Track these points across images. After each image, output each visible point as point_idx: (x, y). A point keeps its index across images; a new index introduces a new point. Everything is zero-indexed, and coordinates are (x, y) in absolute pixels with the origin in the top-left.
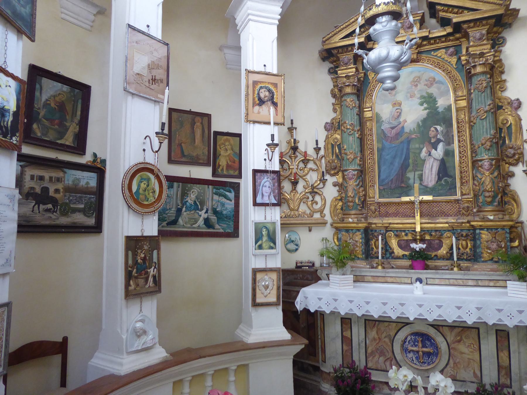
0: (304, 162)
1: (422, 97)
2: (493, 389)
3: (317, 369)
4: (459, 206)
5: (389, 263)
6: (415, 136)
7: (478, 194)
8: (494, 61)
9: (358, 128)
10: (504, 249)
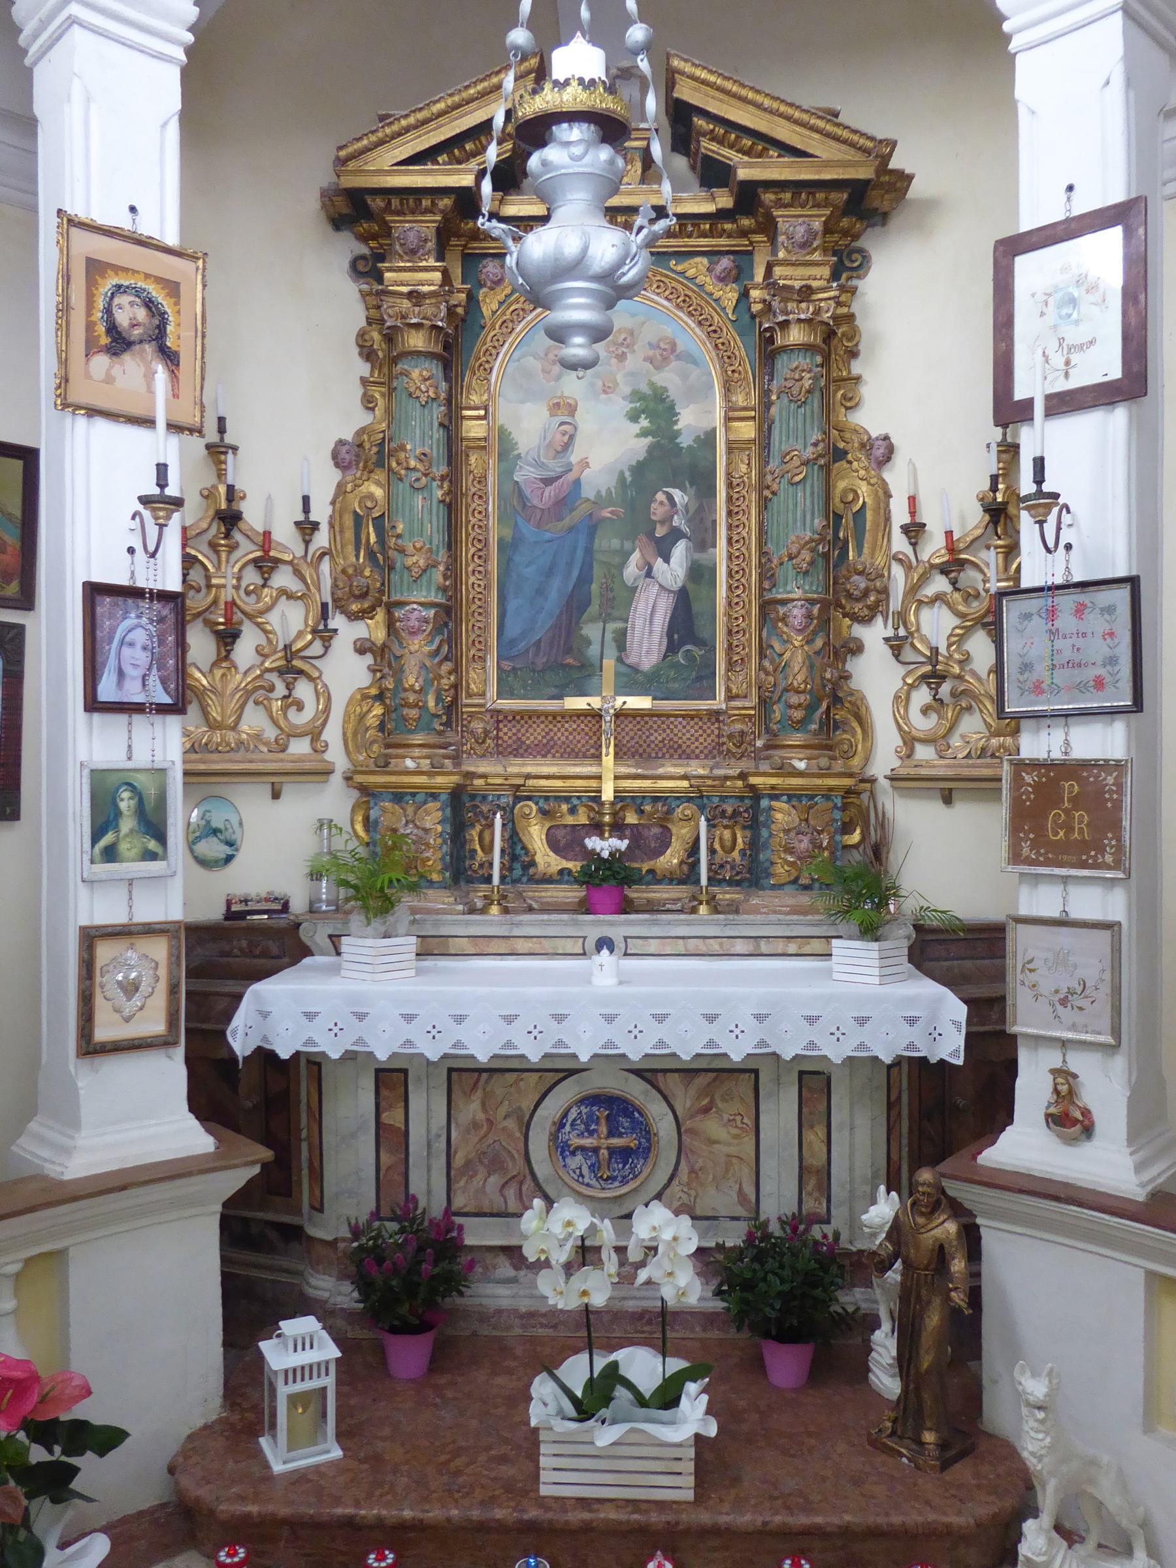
0: (260, 568)
1: (636, 395)
2: (785, 1232)
3: (294, 1234)
4: (719, 728)
5: (520, 895)
6: (611, 512)
7: (771, 698)
8: (835, 317)
9: (443, 469)
10: (826, 854)
